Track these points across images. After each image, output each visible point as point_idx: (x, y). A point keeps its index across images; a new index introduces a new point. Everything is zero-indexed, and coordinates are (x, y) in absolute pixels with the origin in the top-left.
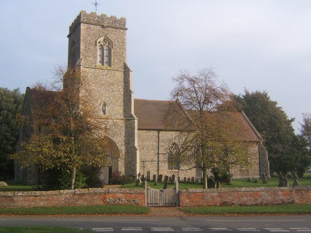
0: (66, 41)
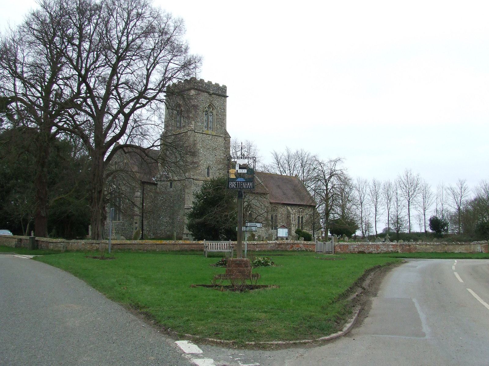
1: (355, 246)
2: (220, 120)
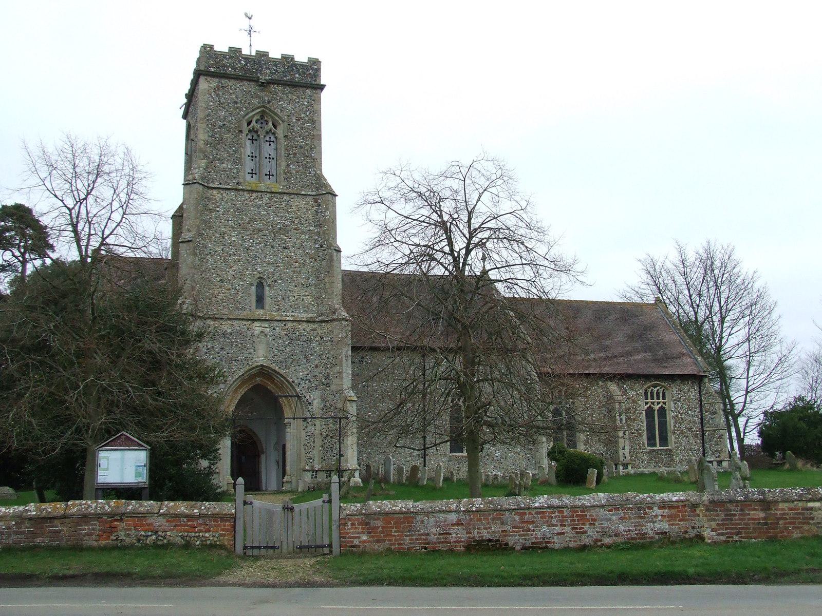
0: (182, 125)
1: (453, 517)
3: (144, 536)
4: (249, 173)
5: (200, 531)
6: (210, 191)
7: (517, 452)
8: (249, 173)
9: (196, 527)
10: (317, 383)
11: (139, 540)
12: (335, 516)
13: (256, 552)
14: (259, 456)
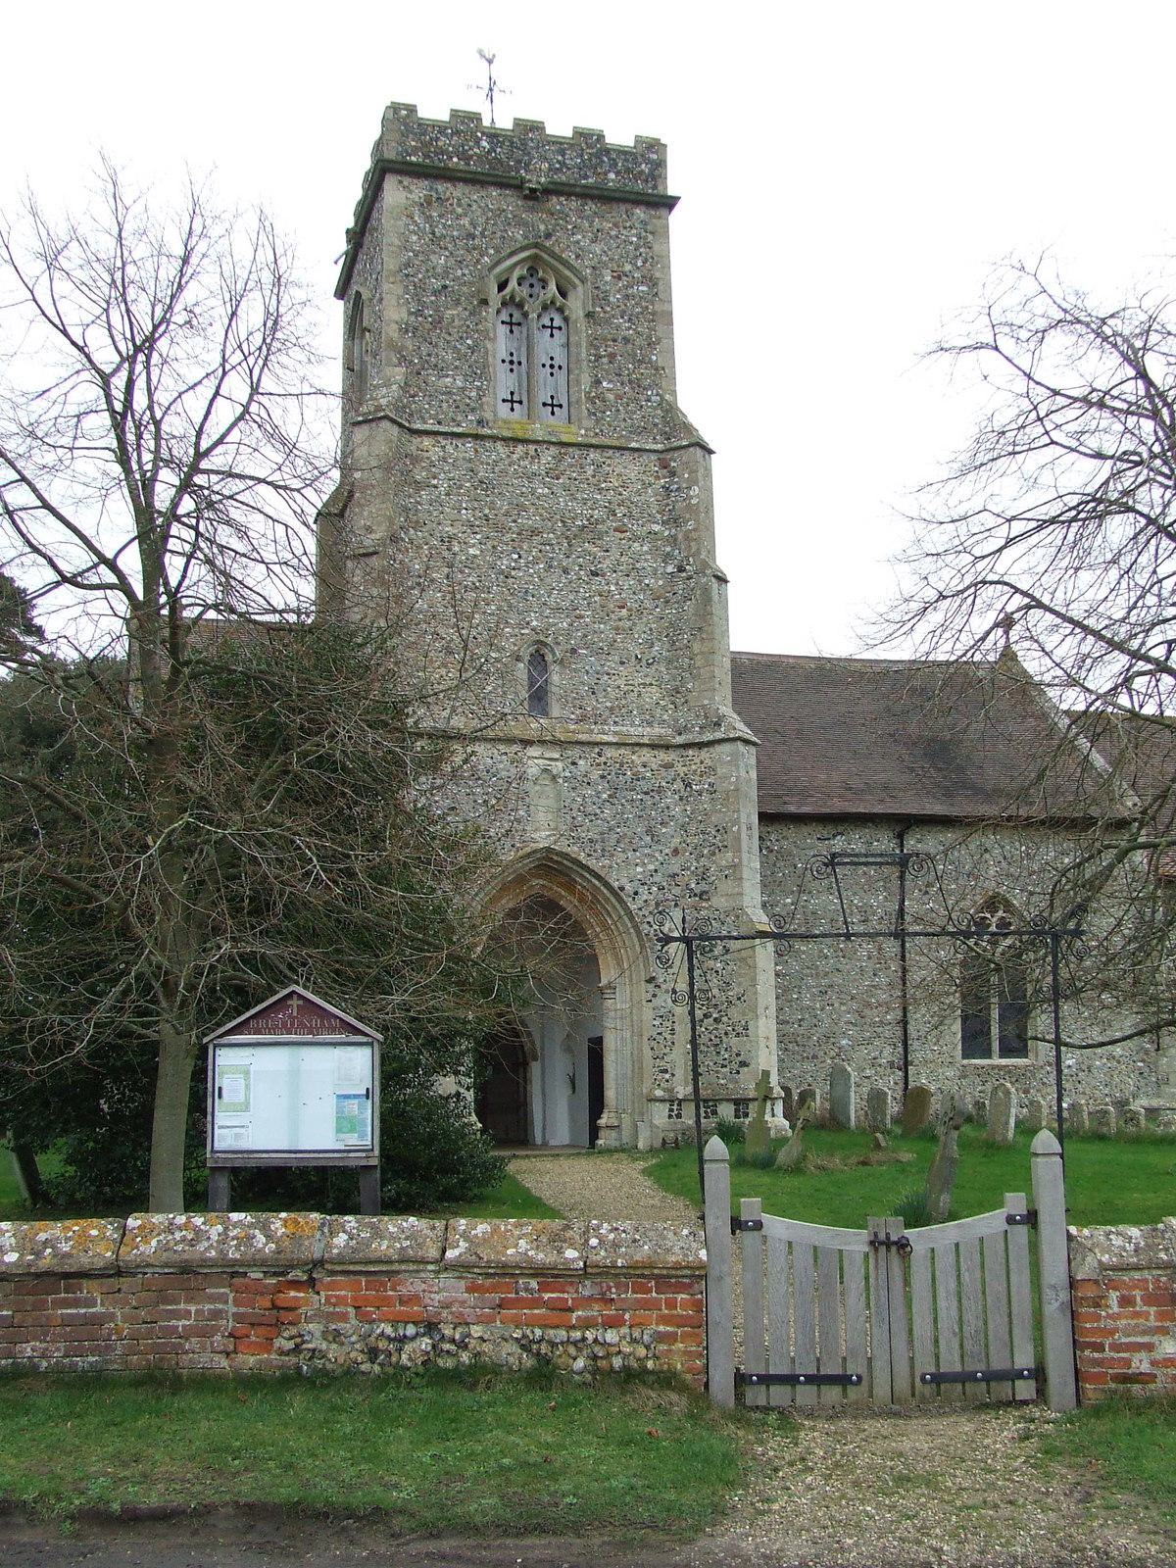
2: (618, 348)
3: (390, 1339)
4: (504, 401)
5: (587, 1324)
6: (416, 440)
7: (1114, 1058)
8: (504, 401)
9: (571, 1310)
10: (676, 891)
11: (373, 1353)
12: (1054, 1270)
13: (779, 1394)
14: (525, 1065)
